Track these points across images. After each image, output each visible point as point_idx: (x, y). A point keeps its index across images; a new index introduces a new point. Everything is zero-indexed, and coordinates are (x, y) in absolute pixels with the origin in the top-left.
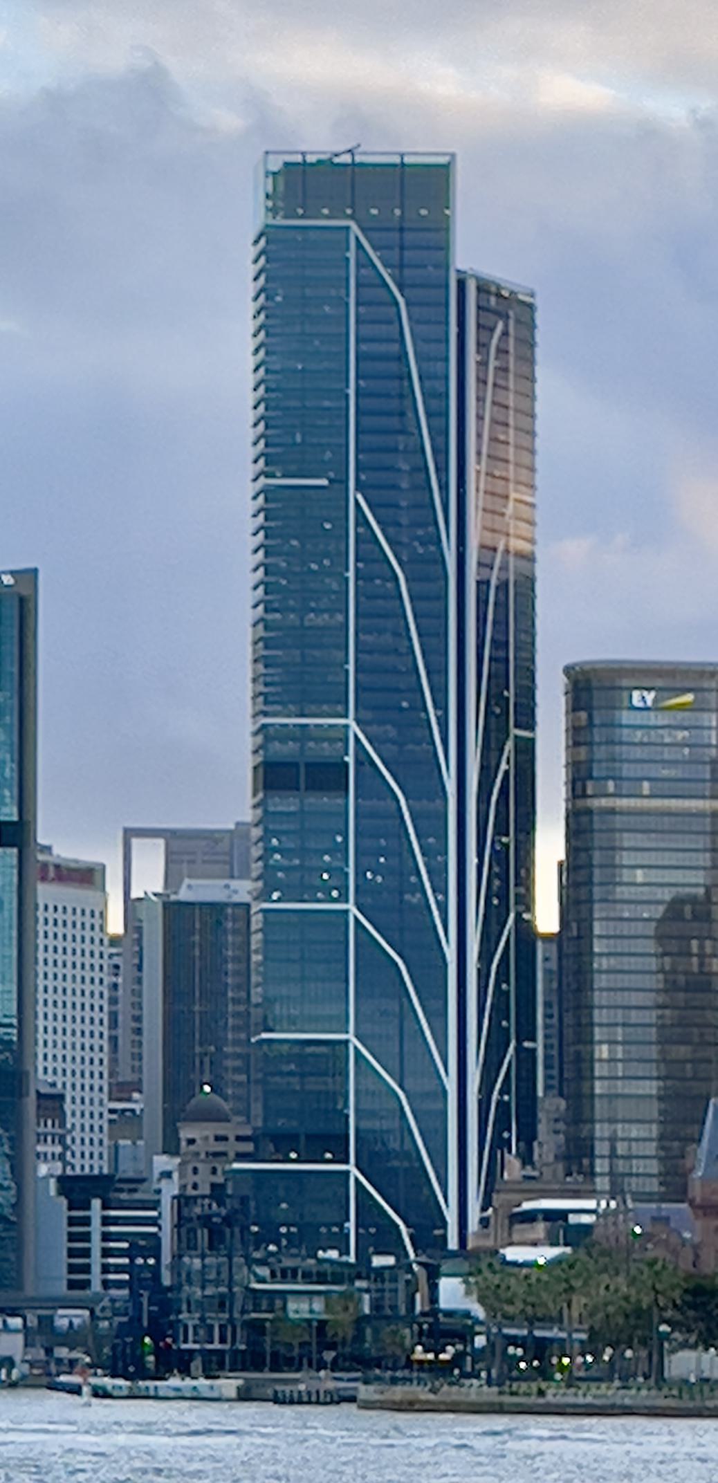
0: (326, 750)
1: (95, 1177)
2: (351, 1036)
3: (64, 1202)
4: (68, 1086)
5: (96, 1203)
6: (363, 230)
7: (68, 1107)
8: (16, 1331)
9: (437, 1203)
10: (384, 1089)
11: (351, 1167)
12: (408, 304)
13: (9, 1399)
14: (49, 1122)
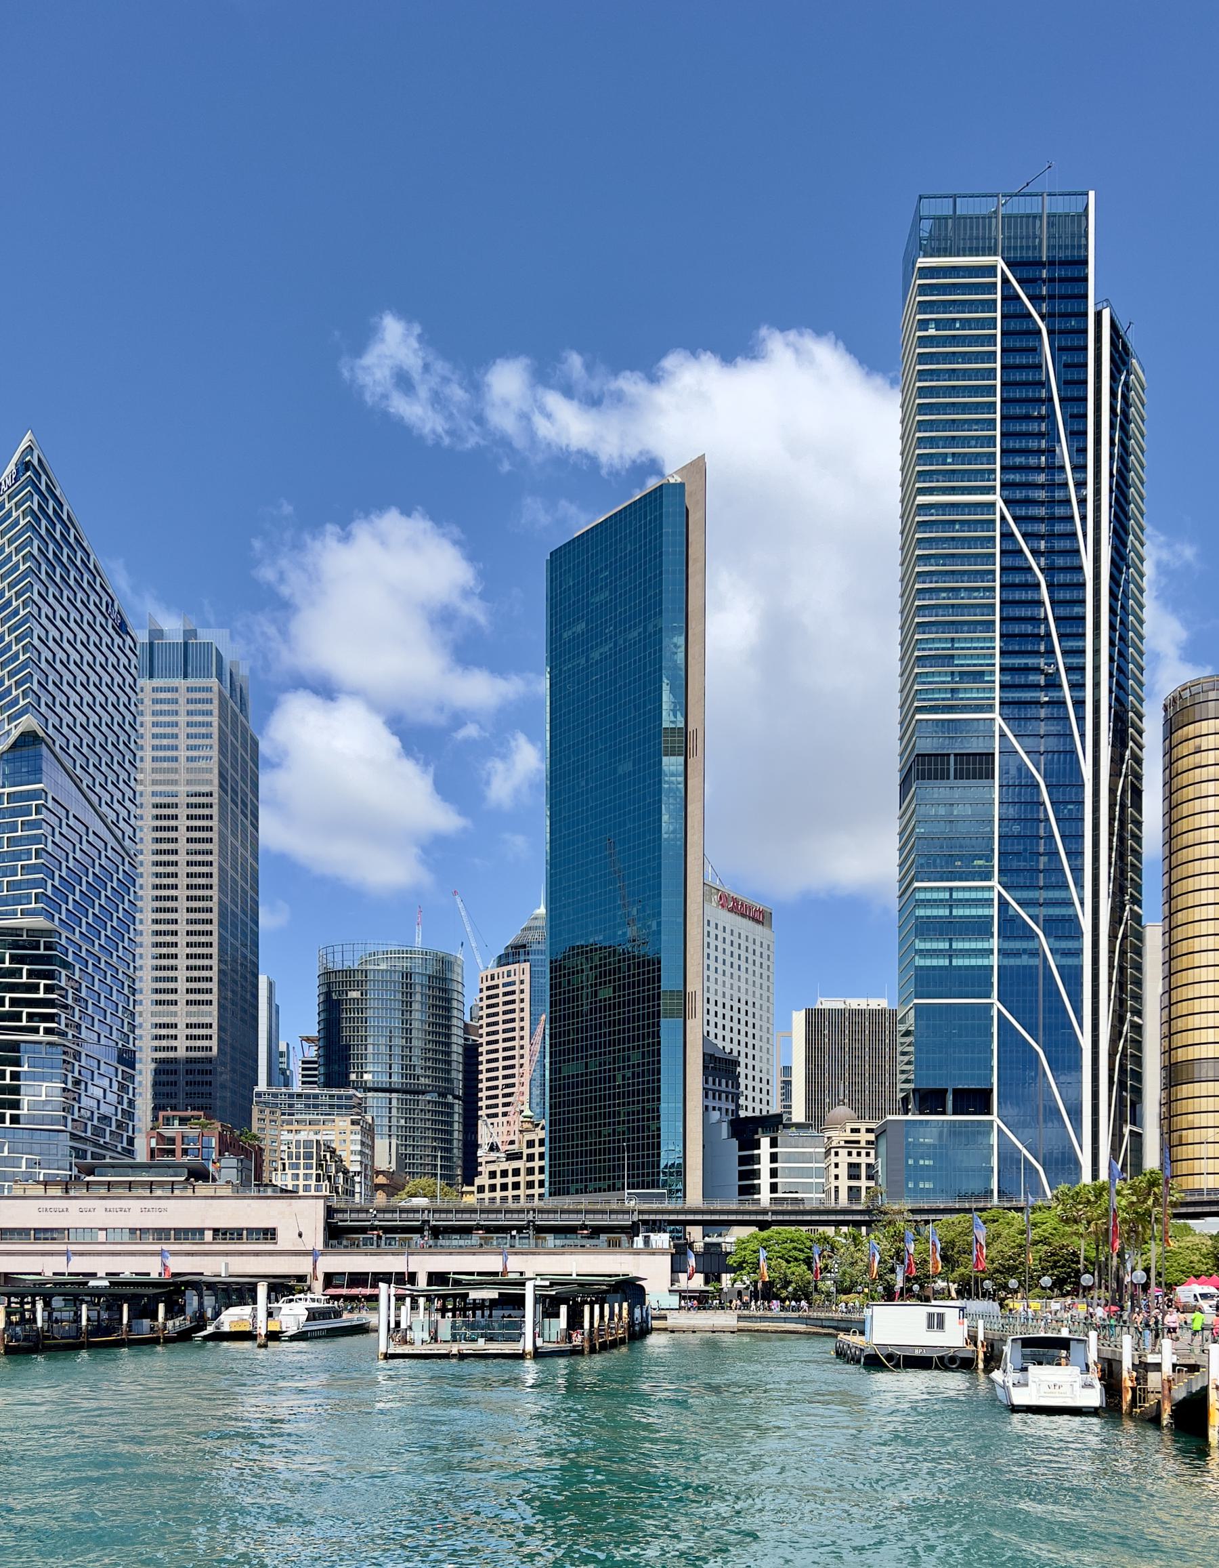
0: (975, 746)
1: (765, 1117)
2: (994, 999)
3: (735, 1143)
4: (743, 1055)
5: (765, 1142)
6: (1009, 264)
7: (741, 1070)
8: (662, 1252)
9: (1072, 1146)
10: (1070, 985)
11: (994, 1117)
12: (1050, 333)
13: (67, 1364)
14: (724, 1081)
